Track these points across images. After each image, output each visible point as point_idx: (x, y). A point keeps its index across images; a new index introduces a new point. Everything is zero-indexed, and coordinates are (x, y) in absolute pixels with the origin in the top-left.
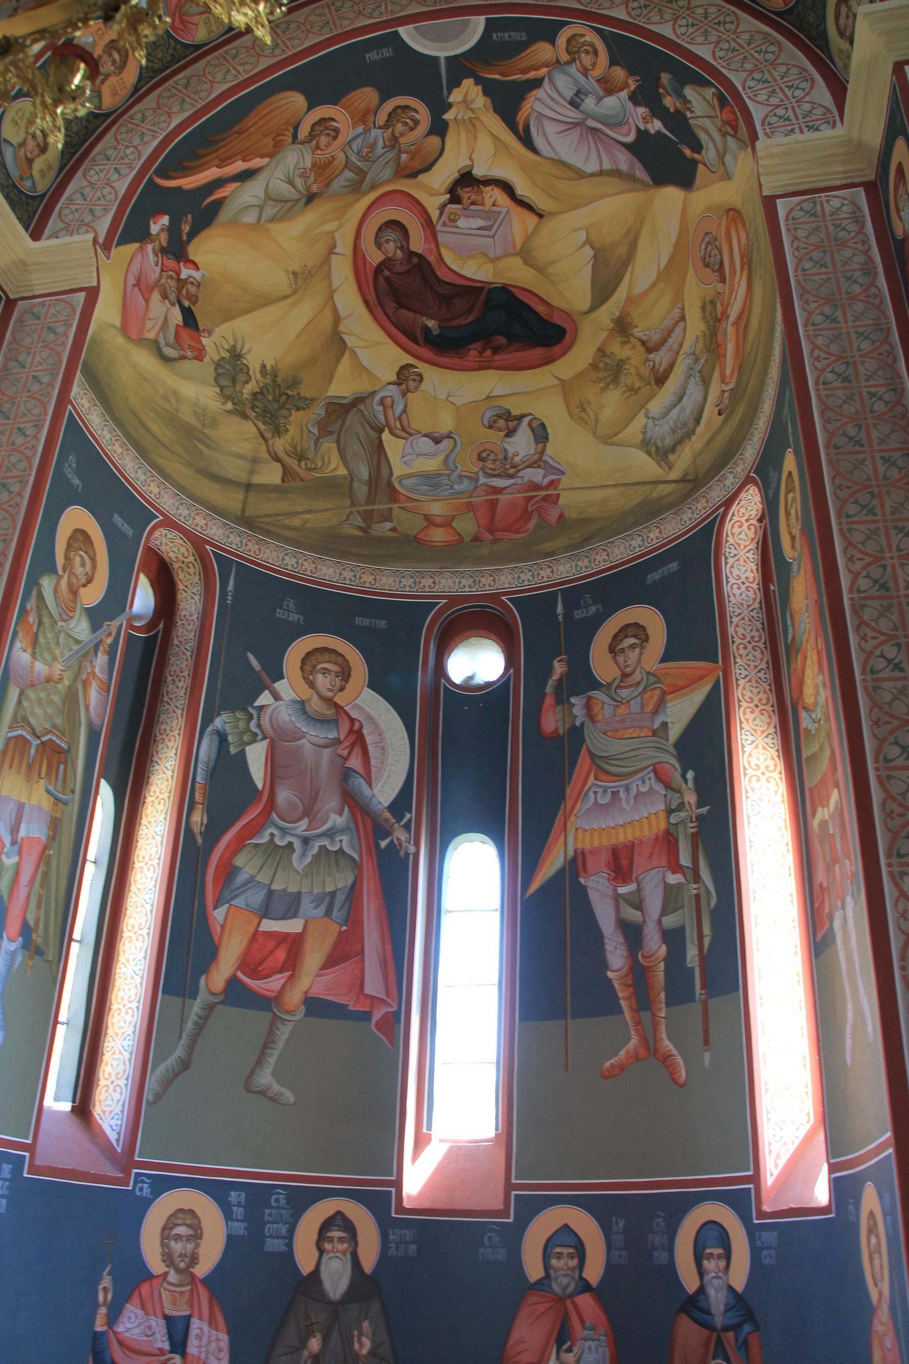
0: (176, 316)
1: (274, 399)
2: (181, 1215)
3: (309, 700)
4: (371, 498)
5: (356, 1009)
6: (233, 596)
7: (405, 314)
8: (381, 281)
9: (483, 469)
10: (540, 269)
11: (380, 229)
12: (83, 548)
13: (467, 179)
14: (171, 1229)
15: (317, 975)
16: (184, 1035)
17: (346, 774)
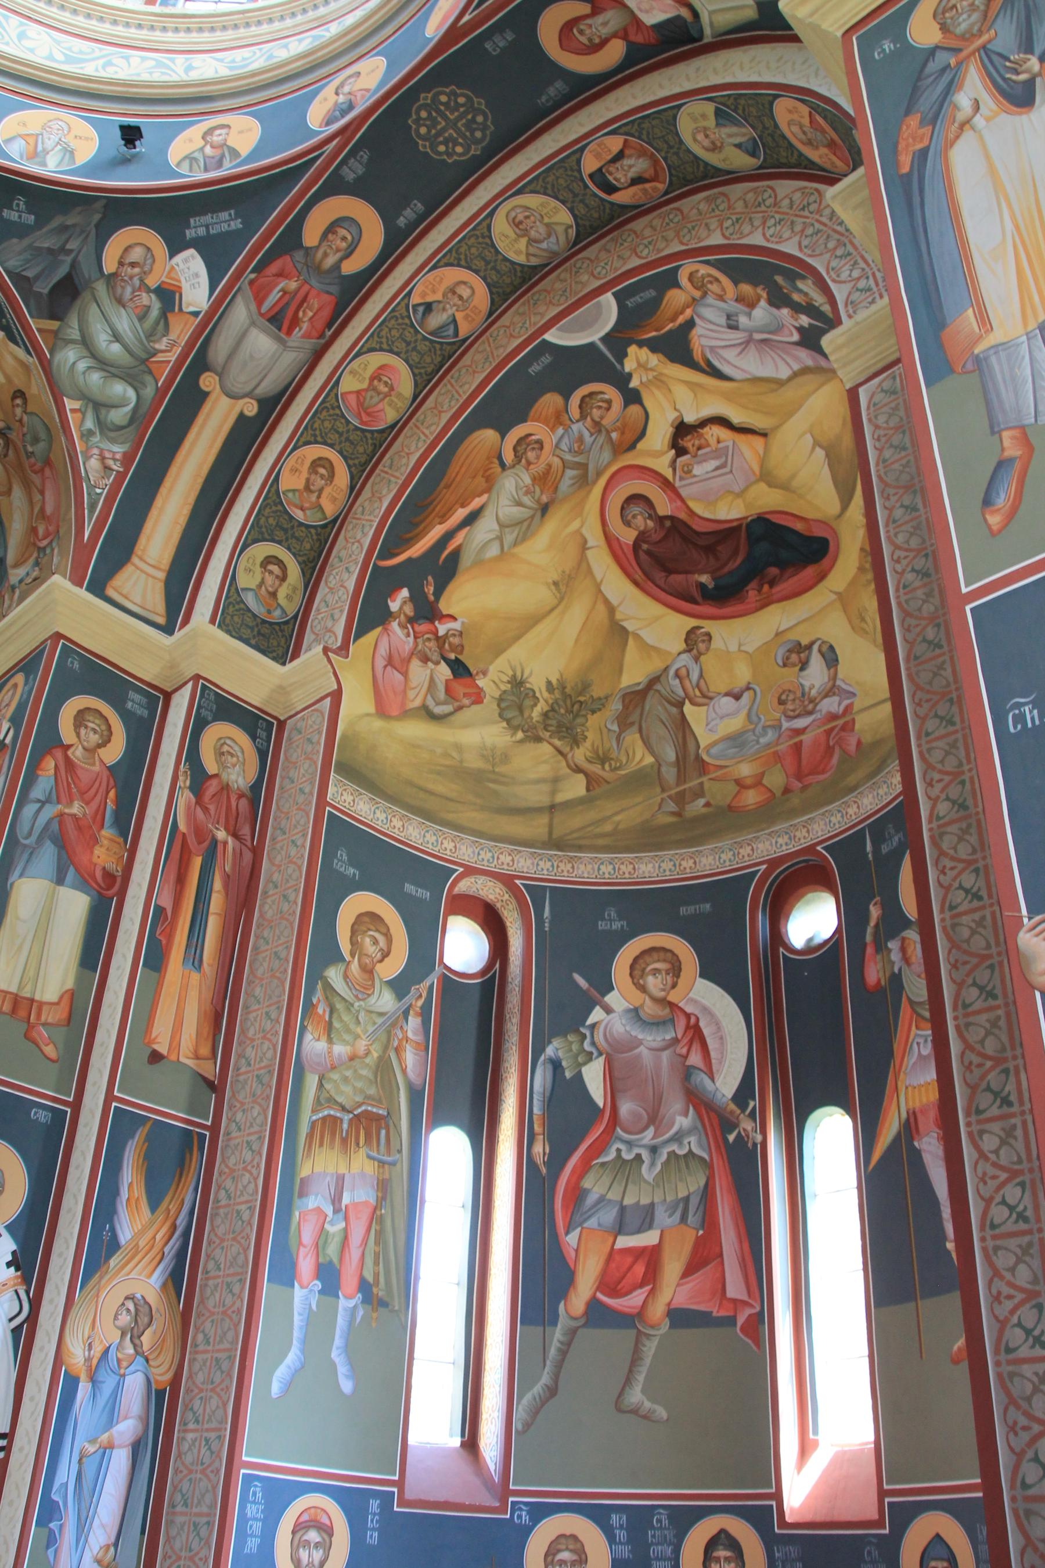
0: (444, 671)
1: (567, 711)
2: (563, 1541)
3: (642, 1006)
4: (681, 778)
5: (719, 1315)
6: (550, 923)
7: (677, 579)
8: (643, 556)
9: (784, 713)
10: (785, 487)
11: (623, 508)
12: (372, 927)
13: (682, 430)
14: (555, 1555)
15: (678, 1285)
16: (548, 1363)
17: (687, 1072)
